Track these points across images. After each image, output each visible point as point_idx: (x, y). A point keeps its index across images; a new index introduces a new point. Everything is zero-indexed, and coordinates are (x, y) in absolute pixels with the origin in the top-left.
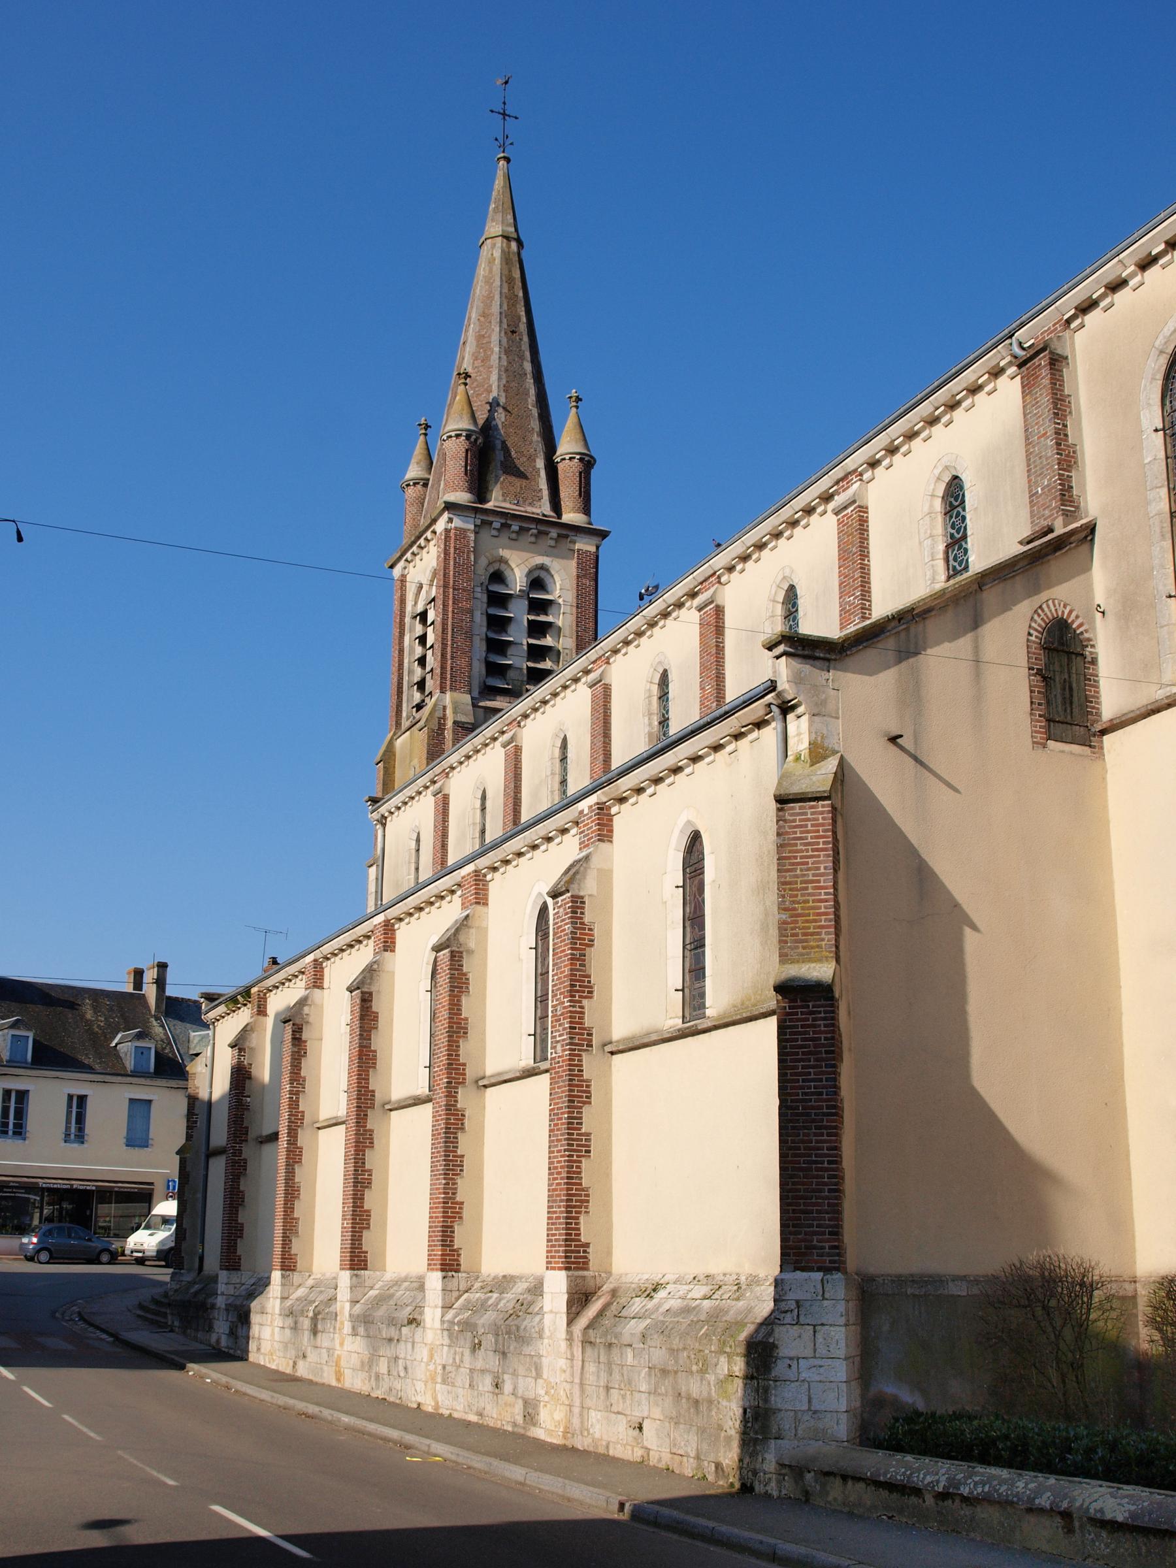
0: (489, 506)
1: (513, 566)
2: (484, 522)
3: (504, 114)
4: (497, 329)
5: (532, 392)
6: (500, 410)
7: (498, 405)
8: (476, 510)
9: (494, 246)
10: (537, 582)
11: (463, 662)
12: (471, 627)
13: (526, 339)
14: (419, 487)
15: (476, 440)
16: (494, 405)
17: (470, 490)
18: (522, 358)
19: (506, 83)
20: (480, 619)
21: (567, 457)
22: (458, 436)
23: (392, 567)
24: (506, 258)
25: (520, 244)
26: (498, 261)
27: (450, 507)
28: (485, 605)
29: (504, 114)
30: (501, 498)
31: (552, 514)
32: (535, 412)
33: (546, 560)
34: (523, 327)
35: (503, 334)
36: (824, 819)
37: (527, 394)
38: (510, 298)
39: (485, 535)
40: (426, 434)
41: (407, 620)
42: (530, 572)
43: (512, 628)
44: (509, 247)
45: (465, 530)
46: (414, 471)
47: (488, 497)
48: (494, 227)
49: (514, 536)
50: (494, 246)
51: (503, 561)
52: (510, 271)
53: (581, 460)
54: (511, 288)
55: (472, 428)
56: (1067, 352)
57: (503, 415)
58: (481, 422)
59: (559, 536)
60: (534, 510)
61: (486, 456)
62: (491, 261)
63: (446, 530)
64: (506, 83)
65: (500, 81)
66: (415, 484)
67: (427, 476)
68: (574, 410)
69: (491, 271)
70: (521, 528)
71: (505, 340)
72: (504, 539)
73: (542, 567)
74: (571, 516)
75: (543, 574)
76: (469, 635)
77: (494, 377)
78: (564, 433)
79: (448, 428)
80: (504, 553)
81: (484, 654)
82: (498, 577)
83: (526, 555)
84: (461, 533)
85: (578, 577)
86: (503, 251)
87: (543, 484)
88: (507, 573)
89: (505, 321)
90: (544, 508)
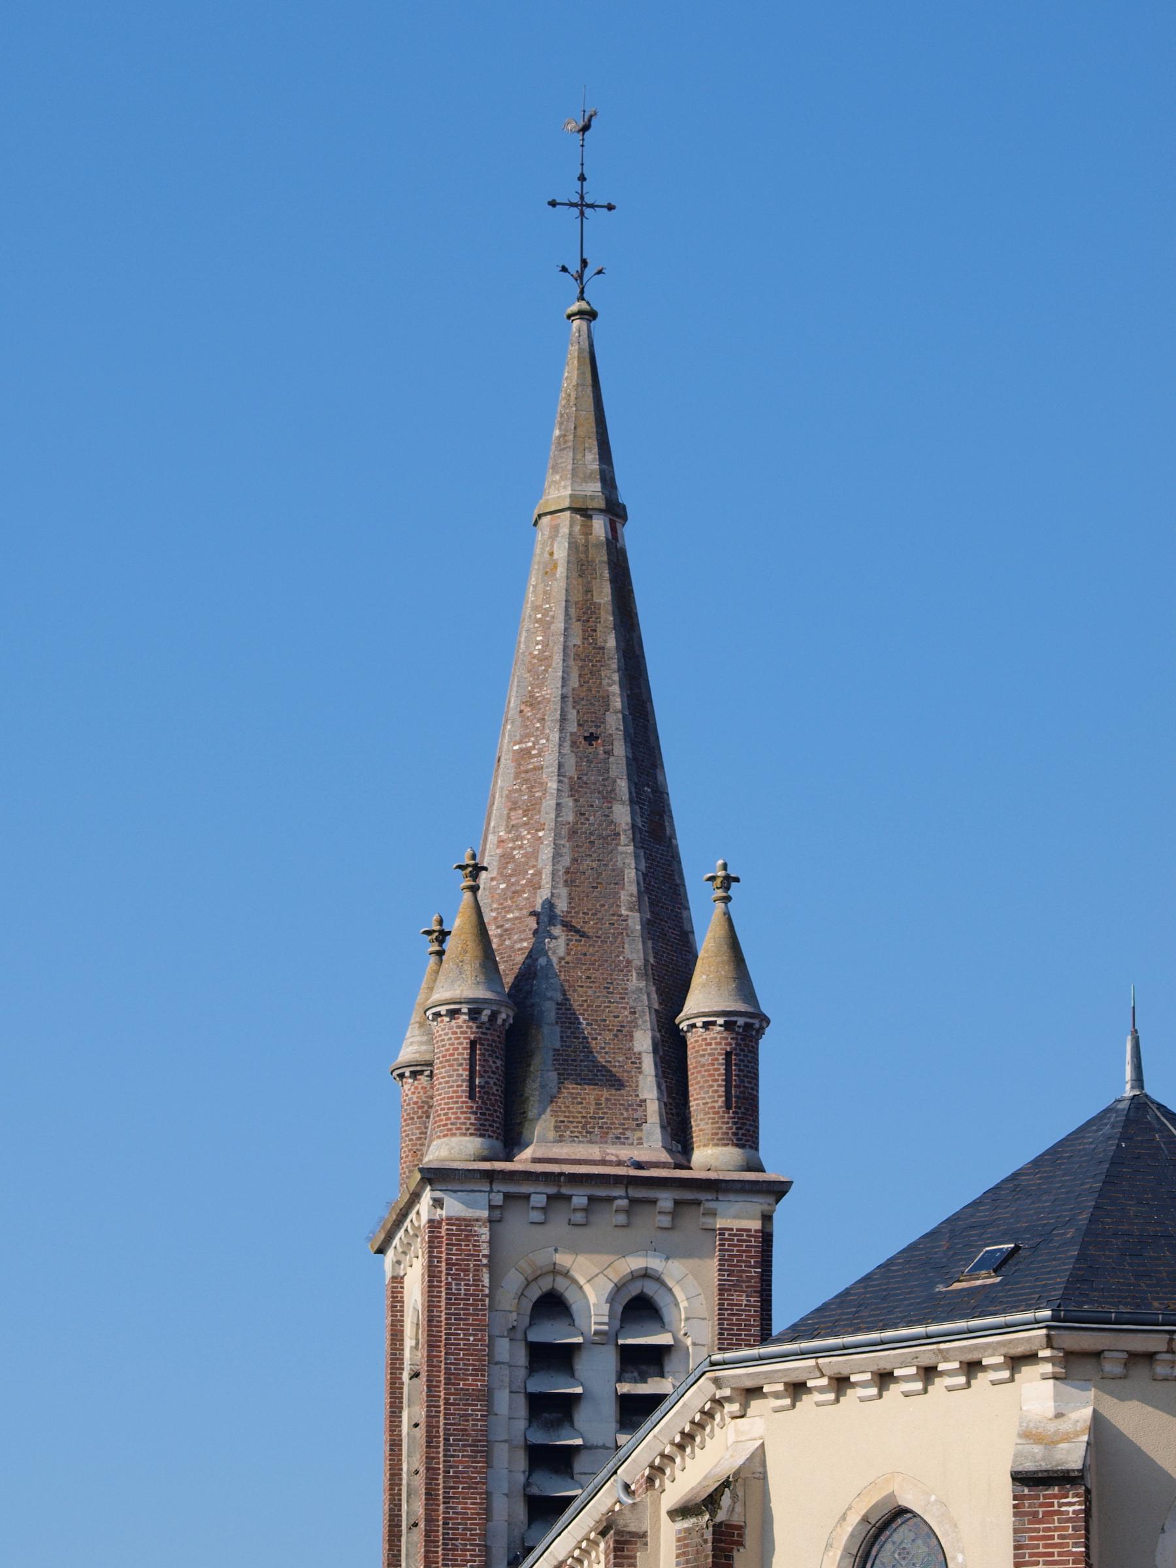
1: (582, 1281)
2: (507, 1196)
3: (582, 205)
4: (555, 737)
6: (557, 930)
8: (490, 1176)
9: (555, 529)
10: (639, 1306)
11: (470, 1507)
12: (486, 1431)
13: (620, 749)
15: (493, 1016)
16: (546, 917)
18: (609, 797)
19: (585, 128)
20: (509, 1409)
21: (699, 1022)
22: (453, 1014)
23: (381, 1251)
24: (580, 565)
25: (615, 511)
26: (561, 571)
27: (435, 1177)
28: (522, 1373)
29: (582, 205)
30: (551, 1135)
31: (664, 1157)
32: (635, 922)
33: (655, 1263)
34: (614, 723)
35: (567, 749)
37: (619, 882)
38: (584, 659)
39: (517, 1224)
41: (405, 1376)
42: (619, 1288)
43: (582, 1416)
44: (587, 531)
45: (468, 1222)
46: (410, 1050)
47: (526, 1133)
48: (559, 492)
49: (579, 1217)
50: (555, 529)
51: (555, 1271)
52: (588, 591)
53: (728, 1026)
54: (590, 632)
55: (482, 993)
56: (647, 1526)
57: (562, 942)
58: (509, 971)
59: (677, 1203)
61: (519, 1047)
62: (549, 571)
64: (585, 128)
71: (570, 762)
72: (558, 1227)
73: (646, 1274)
74: (711, 1156)
75: (650, 1288)
76: (484, 1449)
77: (546, 853)
79: (437, 996)
80: (563, 1259)
81: (521, 1478)
82: (552, 1305)
83: (606, 1259)
84: (462, 1226)
85: (722, 1290)
86: (573, 546)
87: (648, 1088)
88: (571, 1296)
89: (572, 714)
90: (649, 1146)
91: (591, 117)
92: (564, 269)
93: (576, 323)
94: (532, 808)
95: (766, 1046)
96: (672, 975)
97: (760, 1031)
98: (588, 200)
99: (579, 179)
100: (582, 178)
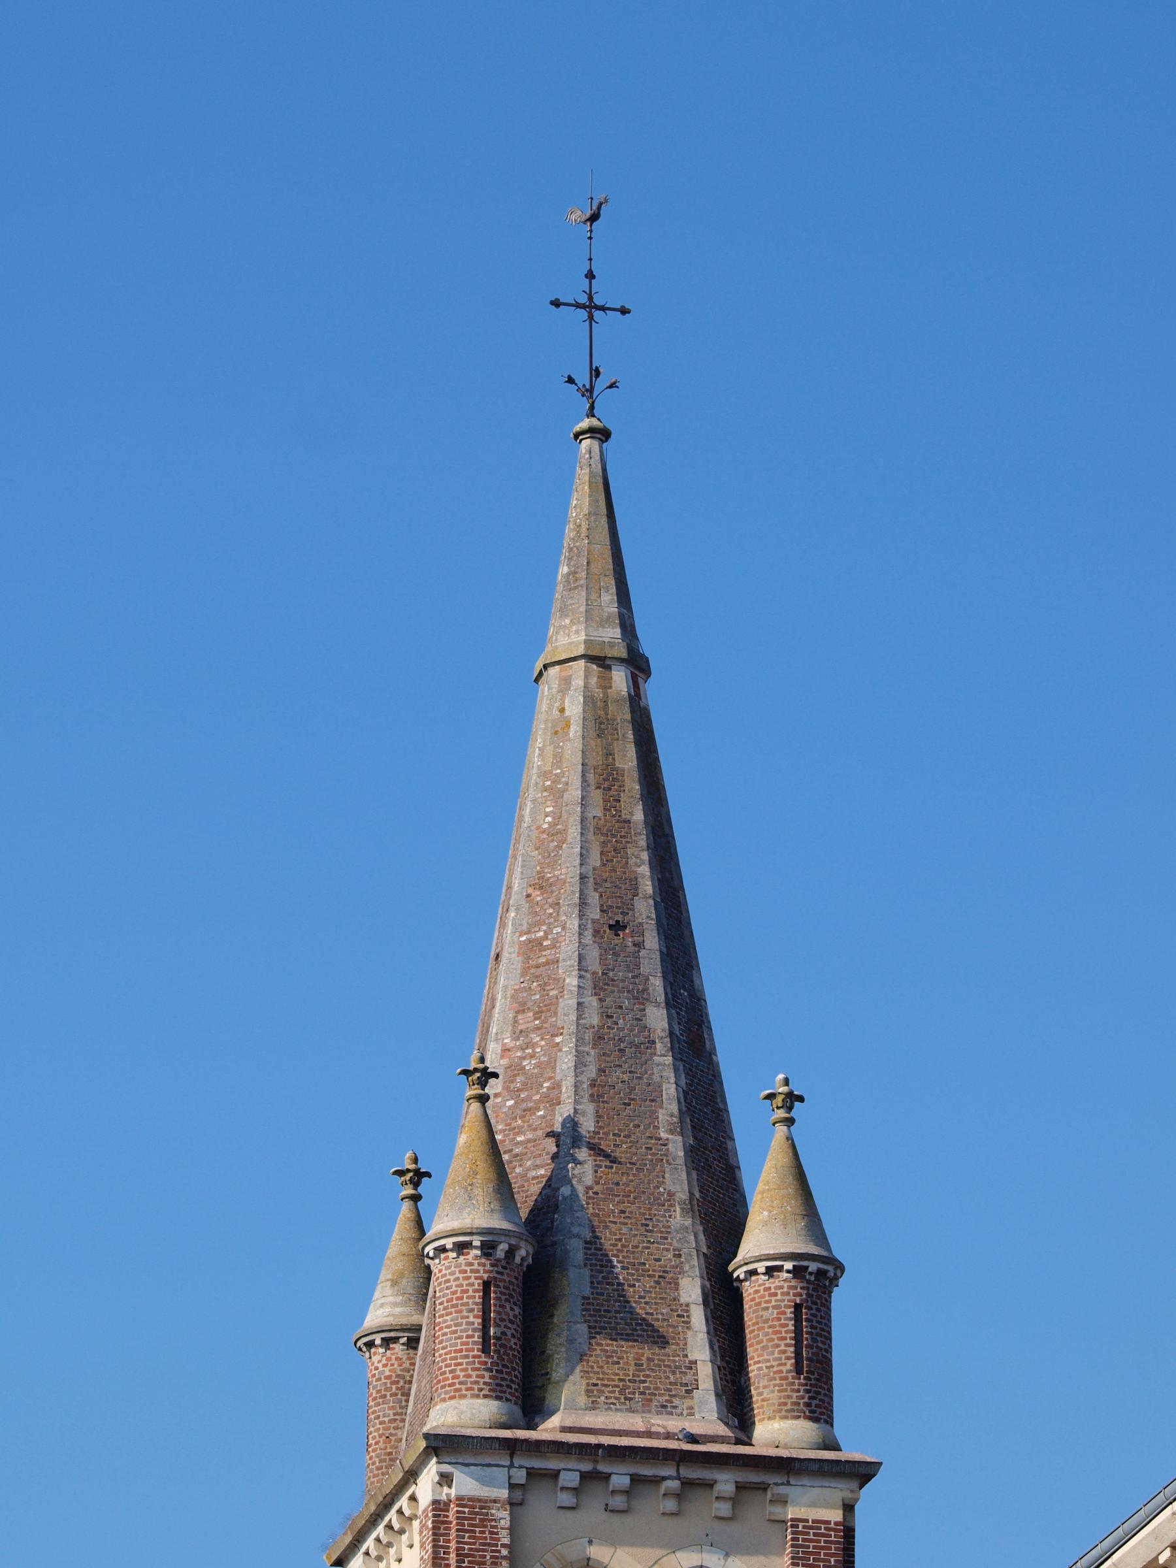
0: (549, 1429)
3: (591, 307)
4: (574, 924)
6: (583, 1154)
7: (576, 1140)
8: (512, 1446)
9: (566, 682)
13: (652, 941)
14: (398, 1348)
15: (510, 1253)
16: (568, 1139)
17: (497, 1392)
18: (641, 997)
19: (594, 218)
21: (761, 1267)
22: (461, 1248)
24: (598, 721)
25: (638, 665)
26: (575, 730)
27: (442, 1445)
29: (591, 307)
30: (582, 1400)
31: (722, 1430)
32: (677, 1147)
34: (644, 910)
35: (588, 938)
37: (656, 1099)
39: (543, 1509)
40: (416, 1198)
46: (384, 1308)
47: (550, 1399)
49: (618, 1501)
50: (566, 682)
52: (609, 754)
53: (797, 1272)
54: (612, 803)
57: (588, 1168)
58: (525, 1202)
59: (740, 1487)
62: (560, 729)
63: (435, 1502)
64: (594, 218)
65: (578, 215)
66: (387, 1342)
67: (415, 1319)
68: (781, 1129)
69: (558, 758)
70: (636, 1479)
71: (593, 953)
72: (592, 1514)
74: (777, 1431)
77: (566, 1062)
84: (474, 1509)
86: (589, 700)
87: (698, 1346)
89: (594, 898)
90: (704, 1416)
91: (601, 204)
92: (571, 380)
93: (586, 443)
94: (546, 1009)
95: (840, 1298)
97: (834, 1281)
98: (598, 301)
99: (586, 276)
100: (590, 276)
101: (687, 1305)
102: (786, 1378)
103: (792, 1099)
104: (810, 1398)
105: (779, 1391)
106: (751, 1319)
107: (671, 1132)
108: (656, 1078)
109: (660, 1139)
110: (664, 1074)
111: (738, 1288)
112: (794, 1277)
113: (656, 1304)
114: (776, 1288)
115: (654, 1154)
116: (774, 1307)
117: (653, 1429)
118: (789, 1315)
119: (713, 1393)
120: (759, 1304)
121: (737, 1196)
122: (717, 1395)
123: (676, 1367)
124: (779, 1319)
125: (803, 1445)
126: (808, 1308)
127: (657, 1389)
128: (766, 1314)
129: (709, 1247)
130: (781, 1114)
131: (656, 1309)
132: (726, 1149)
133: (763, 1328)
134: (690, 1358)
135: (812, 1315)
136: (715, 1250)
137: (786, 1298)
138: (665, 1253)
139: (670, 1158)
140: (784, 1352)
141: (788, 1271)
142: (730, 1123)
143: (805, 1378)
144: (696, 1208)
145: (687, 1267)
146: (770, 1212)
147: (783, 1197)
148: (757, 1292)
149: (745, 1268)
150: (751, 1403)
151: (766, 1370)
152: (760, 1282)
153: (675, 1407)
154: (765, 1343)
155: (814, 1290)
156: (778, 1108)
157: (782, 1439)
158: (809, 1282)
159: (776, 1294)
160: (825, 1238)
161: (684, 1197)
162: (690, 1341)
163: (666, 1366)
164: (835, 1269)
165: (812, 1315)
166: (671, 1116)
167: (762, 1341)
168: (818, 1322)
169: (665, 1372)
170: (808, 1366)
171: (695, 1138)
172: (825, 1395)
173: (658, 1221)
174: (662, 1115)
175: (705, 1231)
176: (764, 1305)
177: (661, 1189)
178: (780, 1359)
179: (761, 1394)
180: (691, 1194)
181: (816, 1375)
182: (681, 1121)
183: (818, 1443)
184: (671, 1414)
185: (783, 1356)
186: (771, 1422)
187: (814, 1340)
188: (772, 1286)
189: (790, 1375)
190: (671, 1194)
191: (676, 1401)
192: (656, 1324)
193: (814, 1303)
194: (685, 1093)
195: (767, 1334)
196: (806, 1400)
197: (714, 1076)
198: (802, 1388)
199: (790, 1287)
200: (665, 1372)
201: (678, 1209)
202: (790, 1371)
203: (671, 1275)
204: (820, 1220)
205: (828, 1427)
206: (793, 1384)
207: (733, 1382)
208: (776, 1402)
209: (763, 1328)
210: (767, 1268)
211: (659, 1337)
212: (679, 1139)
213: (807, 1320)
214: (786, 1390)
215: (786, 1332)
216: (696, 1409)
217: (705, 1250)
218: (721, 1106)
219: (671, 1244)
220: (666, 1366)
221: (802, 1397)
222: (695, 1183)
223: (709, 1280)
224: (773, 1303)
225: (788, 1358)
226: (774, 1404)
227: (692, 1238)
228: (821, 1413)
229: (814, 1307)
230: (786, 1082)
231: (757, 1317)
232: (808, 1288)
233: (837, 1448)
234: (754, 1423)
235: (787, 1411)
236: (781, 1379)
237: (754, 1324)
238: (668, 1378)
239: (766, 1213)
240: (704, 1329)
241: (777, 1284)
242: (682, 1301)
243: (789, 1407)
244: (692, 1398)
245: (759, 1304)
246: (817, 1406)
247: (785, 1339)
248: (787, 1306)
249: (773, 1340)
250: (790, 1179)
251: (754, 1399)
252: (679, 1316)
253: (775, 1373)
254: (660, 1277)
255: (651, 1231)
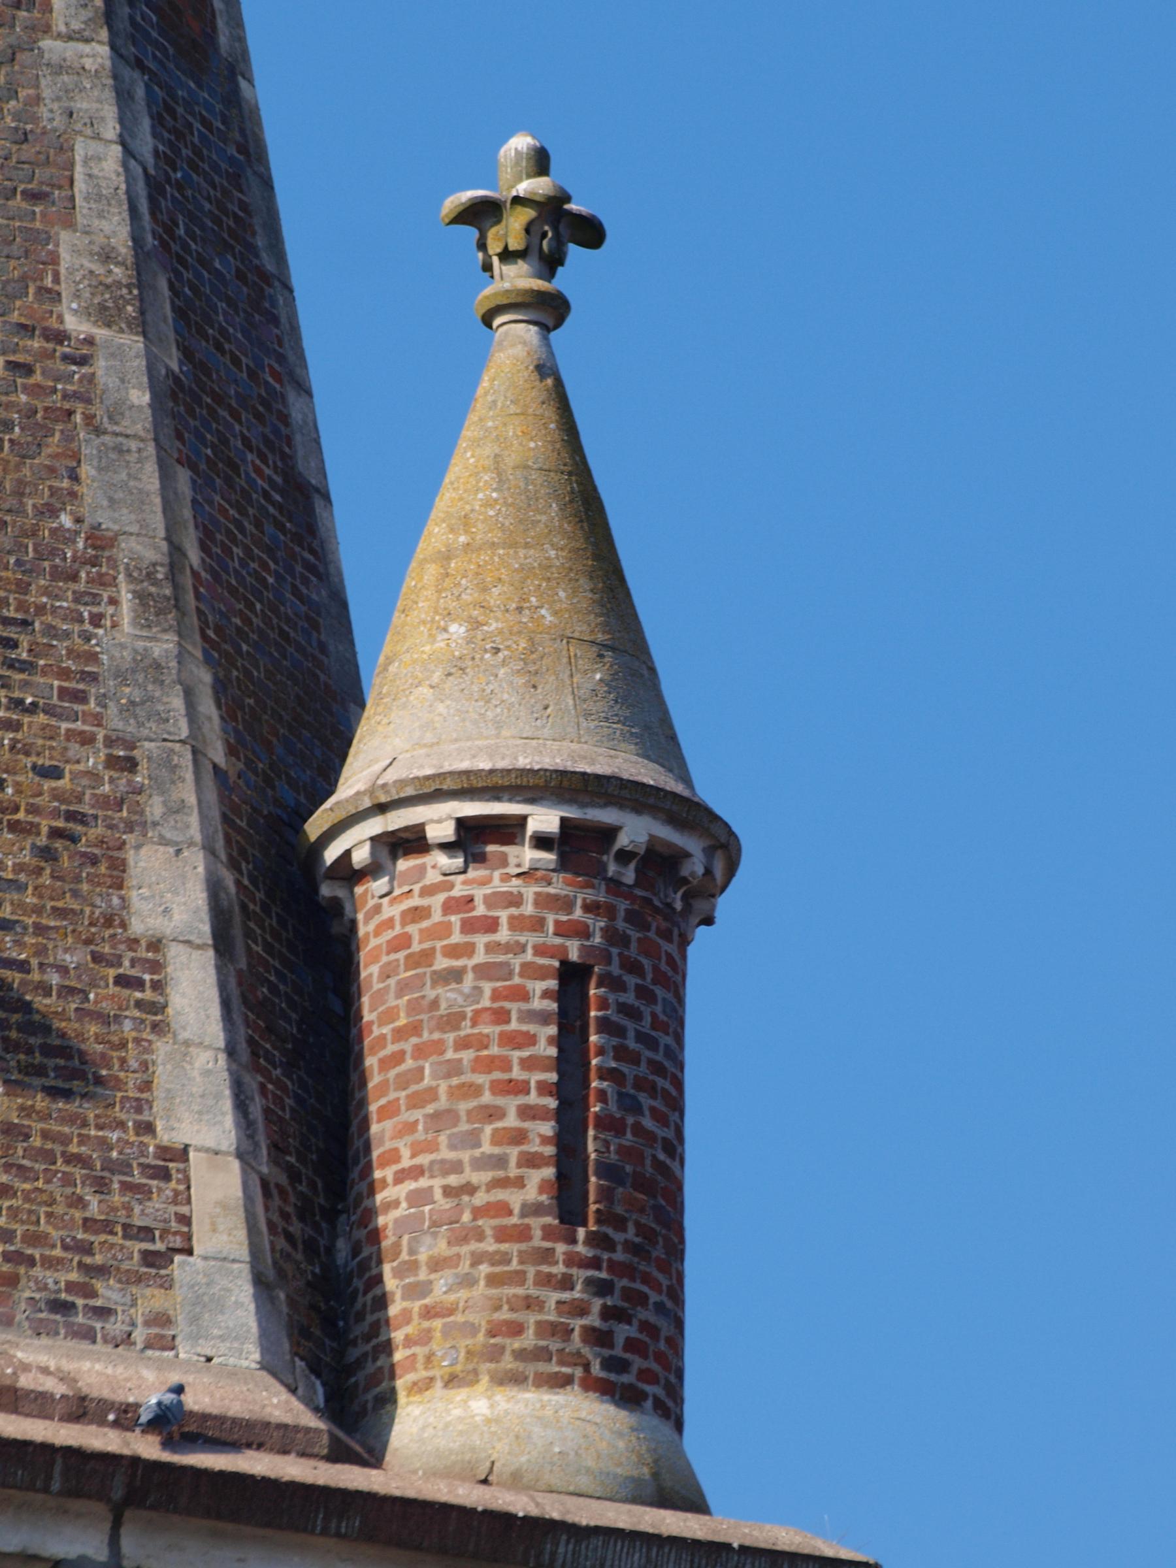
5: (101, 165)
21: (439, 821)
31: (279, 1404)
32: (124, 372)
36: (527, 1112)
37: (49, 192)
53: (575, 847)
60: (99, 1371)
68: (516, 339)
78: (421, 578)
87: (192, 1092)
90: (207, 1350)
95: (713, 962)
96: (288, 687)
97: (699, 902)
101: (156, 945)
102: (523, 1234)
103: (564, 229)
104: (607, 1314)
105: (493, 1280)
106: (389, 1016)
107: (105, 315)
108: (50, 115)
109: (60, 337)
110: (82, 105)
111: (336, 908)
112: (564, 864)
113: (40, 930)
114: (490, 901)
115: (36, 390)
116: (483, 971)
117: (25, 1381)
118: (538, 1004)
119: (243, 1271)
120: (426, 957)
121: (319, 595)
122: (259, 1281)
123: (111, 1167)
124: (502, 1016)
125: (584, 1482)
126: (611, 982)
127: (36, 1239)
128: (449, 996)
129: (231, 751)
130: (518, 277)
131: (41, 951)
132: (285, 419)
133: (438, 1047)
134: (164, 1136)
135: (623, 1008)
136: (249, 763)
137: (531, 939)
138: (74, 749)
139: (99, 411)
140: (519, 1137)
141: (542, 842)
142: (295, 329)
143: (591, 1239)
144: (190, 599)
145: (155, 808)
146: (476, 625)
147: (526, 571)
148: (417, 914)
149: (375, 826)
150: (381, 1325)
151: (443, 1203)
152: (432, 877)
153: (104, 1313)
154: (443, 1102)
155: (631, 917)
156: (507, 256)
157: (503, 1454)
158: (614, 885)
159: (491, 925)
160: (673, 738)
161: (150, 555)
162: (162, 1074)
163: (70, 1159)
164: (709, 852)
165: (623, 1008)
166: (107, 256)
167: (431, 1094)
168: (641, 1037)
169: (68, 1180)
170: (606, 1195)
171: (187, 354)
172: (660, 1308)
173: (50, 631)
174: (70, 250)
175: (220, 688)
176: (442, 963)
177: (66, 520)
178: (500, 1162)
179: (417, 1291)
180: (176, 550)
181: (631, 1233)
182: (142, 282)
183: (637, 1481)
184: (89, 1335)
185: (514, 1152)
186: (461, 1394)
187: (630, 1105)
188: (479, 893)
189: (537, 1224)
190: (100, 541)
191: (108, 1292)
192: (41, 1002)
193: (633, 967)
194: (155, 188)
195: (454, 1069)
196: (593, 1319)
197: (243, 149)
198: (581, 1275)
199: (543, 901)
200: (68, 1180)
201: (126, 597)
202: (535, 1210)
203: (99, 830)
204: (652, 670)
205: (666, 1429)
206: (546, 1256)
207: (311, 1248)
208: (480, 1319)
209: (438, 1047)
210: (462, 824)
211: (48, 1051)
212: (134, 343)
213: (605, 1025)
214: (518, 1278)
215: (529, 1064)
216: (181, 1328)
217: (217, 753)
218: (270, 267)
219: (98, 719)
220: (70, 1159)
221: (580, 1310)
222: (187, 513)
223: (233, 865)
224: (480, 957)
225: (531, 1161)
226: (473, 1329)
227: (177, 703)
228: (646, 1376)
229: (631, 980)
230: (540, 162)
231: (413, 1007)
232: (609, 912)
233: (696, 1504)
234: (389, 1399)
235: (520, 1355)
236: (503, 1235)
237: (400, 1034)
238: (79, 1202)
239: (457, 630)
240: (215, 1033)
241: (497, 885)
242: (137, 927)
243: (529, 1339)
244: (167, 1284)
245: (426, 957)
246: (631, 1345)
247: (521, 1088)
248: (529, 971)
249: (473, 1090)
250: (551, 513)
251: (393, 1310)
252: (122, 981)
253: (477, 1212)
254: (56, 833)
255: (26, 667)
